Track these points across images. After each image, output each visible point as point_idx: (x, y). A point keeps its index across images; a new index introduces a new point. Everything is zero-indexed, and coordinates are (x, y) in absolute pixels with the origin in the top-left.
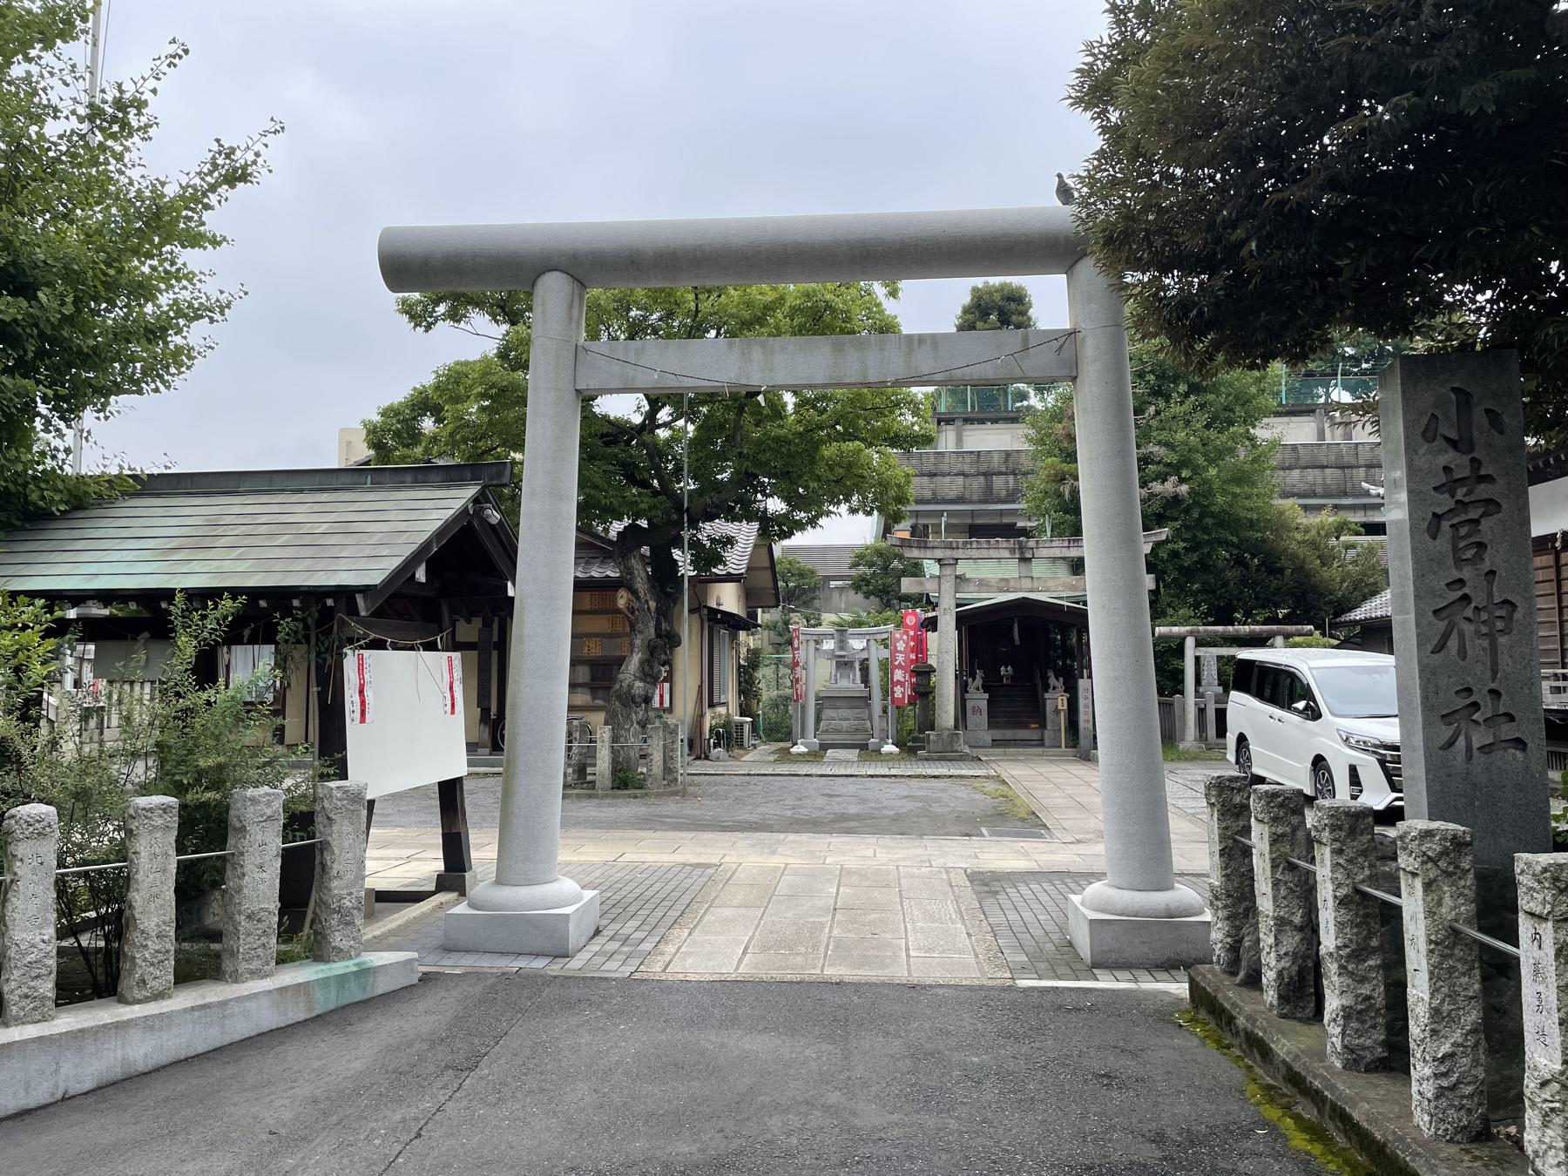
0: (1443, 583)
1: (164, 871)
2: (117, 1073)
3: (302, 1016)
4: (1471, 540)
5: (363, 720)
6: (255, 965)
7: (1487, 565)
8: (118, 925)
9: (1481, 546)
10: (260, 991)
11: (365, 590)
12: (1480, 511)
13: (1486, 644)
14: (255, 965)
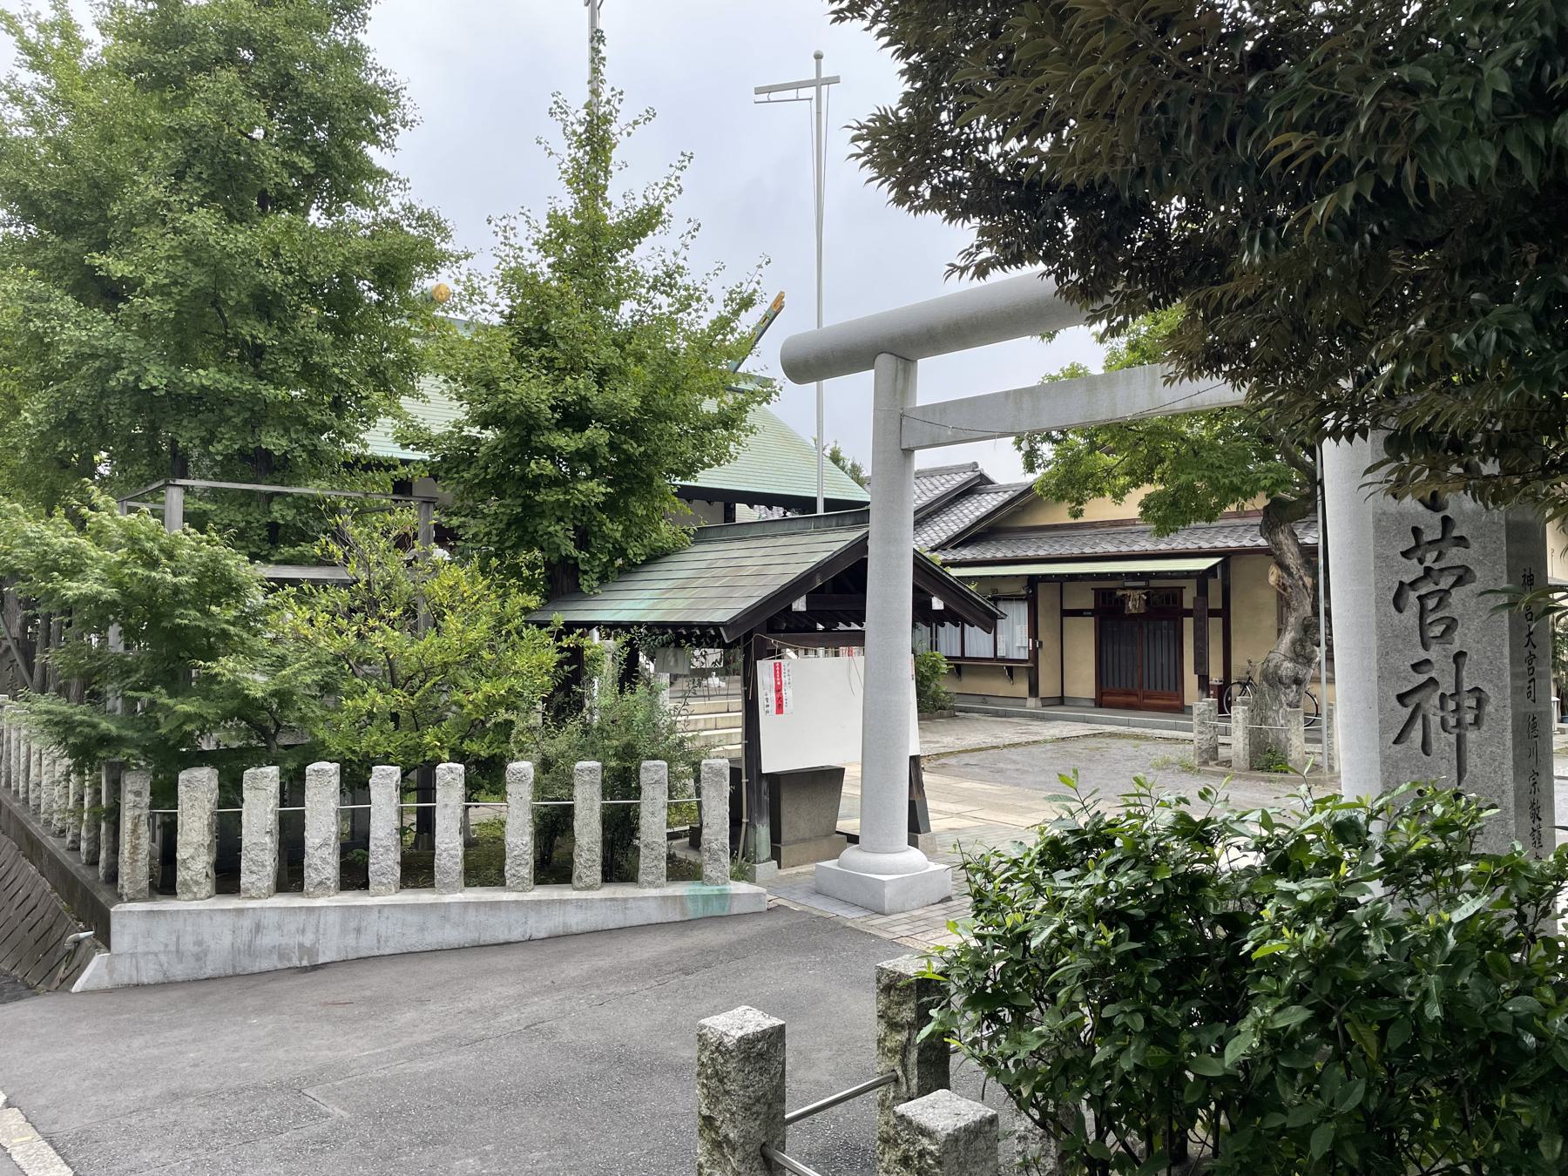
0: (1408, 664)
1: (591, 809)
2: (560, 931)
3: (678, 918)
4: (1439, 615)
5: (780, 709)
6: (650, 878)
7: (1456, 647)
8: (695, 838)
9: (1451, 625)
10: (650, 895)
11: (723, 624)
12: (1452, 580)
13: (1453, 738)
14: (650, 878)
